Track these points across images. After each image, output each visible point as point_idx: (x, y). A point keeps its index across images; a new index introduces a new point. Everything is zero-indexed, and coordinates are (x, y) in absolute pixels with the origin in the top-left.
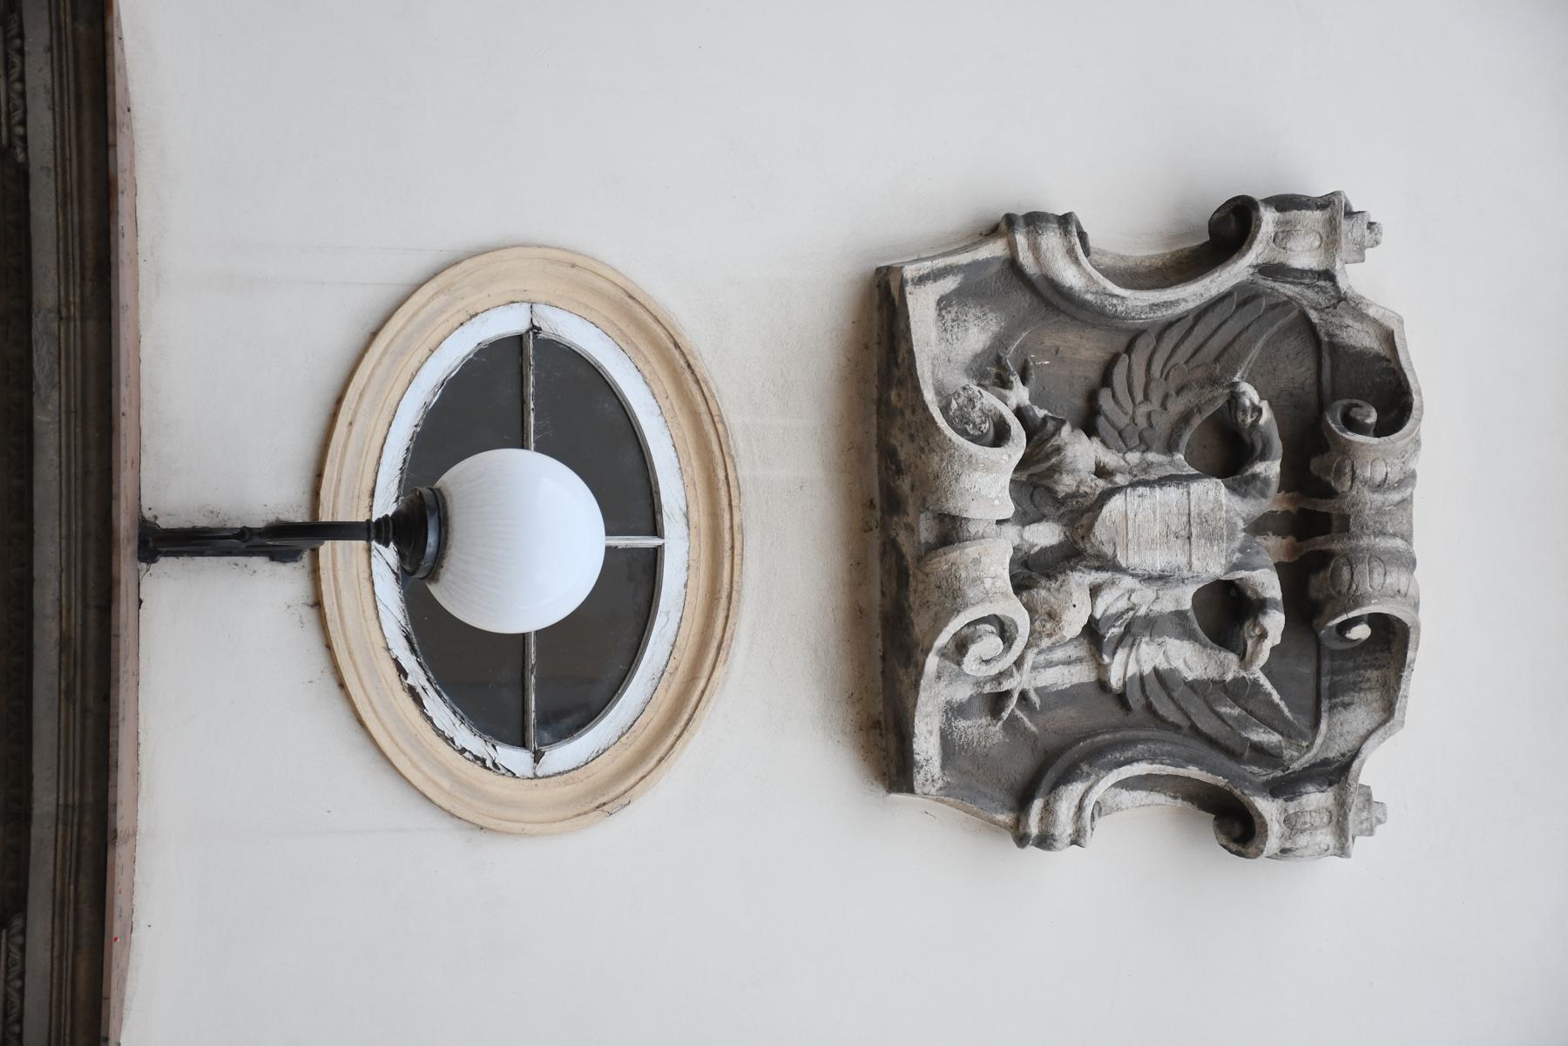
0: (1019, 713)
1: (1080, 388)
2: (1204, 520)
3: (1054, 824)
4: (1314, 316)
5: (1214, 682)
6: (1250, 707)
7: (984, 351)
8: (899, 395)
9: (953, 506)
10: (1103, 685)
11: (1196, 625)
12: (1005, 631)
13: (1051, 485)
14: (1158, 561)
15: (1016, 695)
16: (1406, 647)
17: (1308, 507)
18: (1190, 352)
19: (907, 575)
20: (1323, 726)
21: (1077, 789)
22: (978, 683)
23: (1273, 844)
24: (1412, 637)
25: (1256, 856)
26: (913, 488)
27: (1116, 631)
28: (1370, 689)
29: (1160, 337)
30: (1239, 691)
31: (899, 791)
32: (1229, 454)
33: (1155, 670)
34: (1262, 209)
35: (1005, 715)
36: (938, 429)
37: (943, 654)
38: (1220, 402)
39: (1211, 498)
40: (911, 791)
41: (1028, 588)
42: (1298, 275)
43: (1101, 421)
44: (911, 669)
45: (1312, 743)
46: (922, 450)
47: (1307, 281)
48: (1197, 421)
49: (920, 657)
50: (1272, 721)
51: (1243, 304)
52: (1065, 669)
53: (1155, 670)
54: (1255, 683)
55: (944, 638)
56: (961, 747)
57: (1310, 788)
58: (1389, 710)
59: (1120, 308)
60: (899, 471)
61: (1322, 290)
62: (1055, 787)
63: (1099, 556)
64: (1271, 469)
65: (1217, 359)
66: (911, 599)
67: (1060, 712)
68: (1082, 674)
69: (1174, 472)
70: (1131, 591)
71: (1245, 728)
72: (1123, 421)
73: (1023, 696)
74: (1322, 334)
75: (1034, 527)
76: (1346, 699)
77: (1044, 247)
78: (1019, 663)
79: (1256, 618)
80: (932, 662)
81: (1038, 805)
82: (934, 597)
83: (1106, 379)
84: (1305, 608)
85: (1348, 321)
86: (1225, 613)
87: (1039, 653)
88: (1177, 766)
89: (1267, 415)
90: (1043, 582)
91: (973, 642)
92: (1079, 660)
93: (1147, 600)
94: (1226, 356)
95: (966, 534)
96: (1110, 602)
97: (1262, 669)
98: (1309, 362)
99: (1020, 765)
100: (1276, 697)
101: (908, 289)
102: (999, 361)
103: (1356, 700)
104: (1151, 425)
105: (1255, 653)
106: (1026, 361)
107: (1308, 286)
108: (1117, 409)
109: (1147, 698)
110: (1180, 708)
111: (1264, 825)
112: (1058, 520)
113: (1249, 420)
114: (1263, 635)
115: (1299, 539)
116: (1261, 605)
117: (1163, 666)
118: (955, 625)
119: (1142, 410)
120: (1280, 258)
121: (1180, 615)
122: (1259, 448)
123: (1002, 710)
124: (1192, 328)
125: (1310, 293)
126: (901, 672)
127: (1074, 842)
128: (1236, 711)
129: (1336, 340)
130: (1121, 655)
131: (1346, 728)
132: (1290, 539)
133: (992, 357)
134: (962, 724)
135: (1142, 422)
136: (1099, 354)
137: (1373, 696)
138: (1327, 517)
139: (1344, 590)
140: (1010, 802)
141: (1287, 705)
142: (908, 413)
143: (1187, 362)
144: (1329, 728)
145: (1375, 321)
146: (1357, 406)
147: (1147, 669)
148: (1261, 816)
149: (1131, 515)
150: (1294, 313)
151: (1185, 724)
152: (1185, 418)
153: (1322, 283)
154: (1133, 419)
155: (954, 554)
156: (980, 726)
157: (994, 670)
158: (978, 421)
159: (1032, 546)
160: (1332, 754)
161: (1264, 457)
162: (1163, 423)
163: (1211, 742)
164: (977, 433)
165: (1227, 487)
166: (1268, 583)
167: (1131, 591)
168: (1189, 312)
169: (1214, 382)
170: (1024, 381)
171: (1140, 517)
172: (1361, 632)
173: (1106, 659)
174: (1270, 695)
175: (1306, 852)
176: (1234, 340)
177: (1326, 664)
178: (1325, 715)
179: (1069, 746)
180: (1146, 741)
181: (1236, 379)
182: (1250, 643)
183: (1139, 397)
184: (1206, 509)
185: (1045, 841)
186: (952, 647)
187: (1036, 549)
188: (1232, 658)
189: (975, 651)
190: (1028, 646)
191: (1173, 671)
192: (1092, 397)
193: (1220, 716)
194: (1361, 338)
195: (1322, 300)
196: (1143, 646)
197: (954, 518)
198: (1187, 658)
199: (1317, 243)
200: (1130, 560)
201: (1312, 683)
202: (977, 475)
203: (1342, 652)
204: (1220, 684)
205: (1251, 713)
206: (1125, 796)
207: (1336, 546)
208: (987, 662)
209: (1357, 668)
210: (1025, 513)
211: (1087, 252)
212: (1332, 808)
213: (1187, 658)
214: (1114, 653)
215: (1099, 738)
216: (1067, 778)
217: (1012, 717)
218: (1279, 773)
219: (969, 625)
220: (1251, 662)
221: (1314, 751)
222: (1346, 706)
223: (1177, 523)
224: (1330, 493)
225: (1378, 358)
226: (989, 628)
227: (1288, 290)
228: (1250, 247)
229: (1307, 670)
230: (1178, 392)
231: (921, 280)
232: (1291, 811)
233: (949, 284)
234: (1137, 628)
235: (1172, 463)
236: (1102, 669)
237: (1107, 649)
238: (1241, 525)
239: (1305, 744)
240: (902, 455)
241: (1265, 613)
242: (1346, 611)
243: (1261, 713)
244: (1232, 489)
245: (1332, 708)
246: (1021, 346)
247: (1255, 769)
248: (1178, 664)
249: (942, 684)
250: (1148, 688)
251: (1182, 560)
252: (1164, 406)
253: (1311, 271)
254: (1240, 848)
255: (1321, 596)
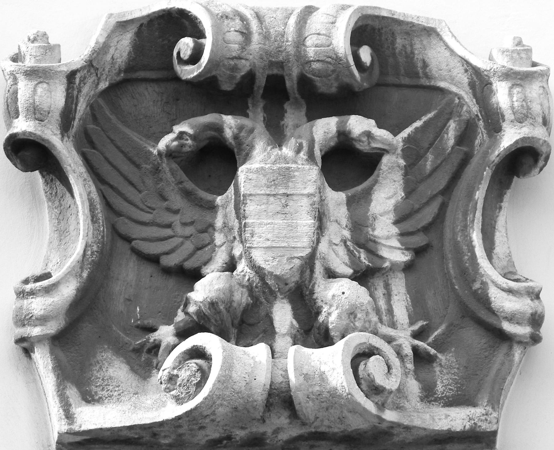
0: (431, 339)
1: (159, 280)
2: (273, 183)
3: (523, 313)
4: (103, 85)
5: (406, 175)
6: (426, 145)
7: (128, 363)
8: (165, 437)
9: (259, 393)
10: (408, 268)
11: (359, 188)
12: (362, 355)
13: (241, 309)
14: (306, 223)
15: (417, 342)
16: (377, 17)
17: (261, 91)
18: (131, 188)
19: (316, 433)
20: (442, 84)
21: (494, 294)
22: (406, 374)
23: (539, 132)
24: (370, 12)
25: (549, 146)
26: (242, 428)
27: (363, 256)
28: (411, 46)
29: (119, 214)
30: (413, 153)
31: (494, 442)
32: (216, 160)
33: (396, 223)
34: (15, 131)
35: (433, 351)
36: (196, 408)
37: (381, 406)
38: (175, 166)
39: (254, 176)
40: (494, 434)
41: (327, 330)
42: (71, 100)
43: (189, 265)
44: (395, 431)
45: (456, 95)
46: (213, 421)
47: (75, 93)
48: (189, 185)
49: (384, 426)
50: (437, 128)
51: (92, 144)
52: (395, 298)
53: (396, 223)
54: (407, 140)
55: (369, 405)
56: (459, 389)
57: (494, 100)
58: (430, 32)
59: (95, 248)
60: (229, 438)
61: (83, 80)
62: (492, 312)
63: (302, 271)
64: (230, 123)
65: (138, 166)
66: (336, 430)
67: (430, 303)
68: (399, 286)
69: (232, 206)
70: (331, 243)
71: (444, 149)
72: (189, 246)
73: (417, 335)
74: (118, 79)
75: (277, 324)
76: (420, 64)
77: (42, 312)
78: (389, 340)
79: (353, 139)
80: (390, 416)
81: (507, 326)
82: (335, 413)
83: (154, 260)
84: (343, 100)
85: (108, 58)
86: (347, 165)
87: (381, 321)
88: (475, 209)
89: (184, 127)
90: (321, 318)
91: (373, 381)
92: (387, 286)
93: (338, 230)
94: (135, 159)
95: (283, 385)
96: (340, 262)
97: (395, 135)
98: (141, 88)
99: (473, 337)
100: (418, 124)
101: (75, 428)
102: (138, 351)
103: (420, 57)
104: (192, 223)
105: (383, 141)
106: (137, 327)
107: (79, 91)
108: (179, 251)
109: (419, 230)
110: (427, 203)
111: (523, 139)
112: (271, 304)
113: (190, 142)
114: (368, 135)
115: (288, 99)
116: (343, 135)
117: (391, 217)
118: (360, 397)
119: (179, 229)
120: (56, 116)
121: (351, 202)
122: (213, 133)
123: (428, 354)
124: (112, 187)
125: (85, 90)
126: (396, 439)
127: (537, 297)
128: (430, 157)
129: (123, 67)
130: (384, 253)
131: (443, 66)
132: (287, 106)
133: (134, 356)
134: (440, 388)
135: (189, 230)
136: (131, 264)
137: (416, 41)
138: (270, 78)
139: (331, 67)
140: (504, 348)
141: (425, 114)
142: (180, 431)
143: (140, 192)
144: (445, 80)
145: (109, 37)
146: (179, 53)
147: (395, 230)
148: (517, 142)
149: (268, 244)
150: (101, 102)
151: (439, 200)
152: (187, 194)
153: (77, 81)
154: (187, 238)
155: (299, 397)
156: (441, 372)
157: (395, 361)
158: (188, 373)
159: (292, 326)
160: (465, 80)
161: (219, 129)
162: (191, 213)
163: (456, 177)
164: (199, 375)
165: (244, 163)
166: (325, 128)
167: (331, 243)
168: (97, 187)
169: (157, 170)
170: (153, 330)
171: (269, 236)
172: (365, 54)
173: (387, 264)
174: (416, 129)
175: (546, 105)
176: (122, 152)
177: (391, 79)
178: (432, 83)
179: (457, 296)
180: (454, 234)
181: (155, 152)
182: (374, 145)
183: (169, 232)
184: (264, 181)
185: (536, 320)
186: (378, 398)
187: (295, 322)
188: (386, 160)
189: (380, 380)
190: (375, 333)
191: (396, 208)
192: (167, 271)
193: (435, 170)
194: (124, 44)
195: (90, 81)
196: (376, 233)
197: (270, 395)
198: (386, 195)
199: (45, 85)
200: (305, 244)
201: (406, 92)
202: (234, 375)
203: (381, 66)
204: (408, 171)
205: (431, 145)
206: (499, 249)
207: (295, 72)
208: (389, 368)
209: (394, 54)
210: (265, 331)
211: (47, 276)
212: (509, 84)
213: (386, 195)
214: (381, 258)
215: (452, 272)
216: (485, 301)
217: (433, 345)
218: (481, 123)
219: (359, 384)
220: (390, 145)
221: (462, 93)
222: (425, 65)
223: (275, 205)
224: (251, 76)
225: (138, 34)
226: (361, 367)
227: (82, 107)
228: (48, 141)
229: (396, 95)
230: (164, 198)
231: (69, 416)
232: (512, 117)
233: (72, 393)
234: (361, 237)
235: (225, 206)
236: (394, 267)
237: (378, 263)
238: (276, 151)
239: (457, 101)
240: (216, 435)
241: (350, 132)
242: (348, 66)
243: (431, 136)
244: (247, 157)
245: (428, 76)
246: (124, 330)
247: (477, 142)
248: (390, 204)
249: (407, 405)
250: (411, 230)
251: (305, 203)
252: (176, 212)
253: (67, 90)
254: (542, 158)
255: (336, 84)
